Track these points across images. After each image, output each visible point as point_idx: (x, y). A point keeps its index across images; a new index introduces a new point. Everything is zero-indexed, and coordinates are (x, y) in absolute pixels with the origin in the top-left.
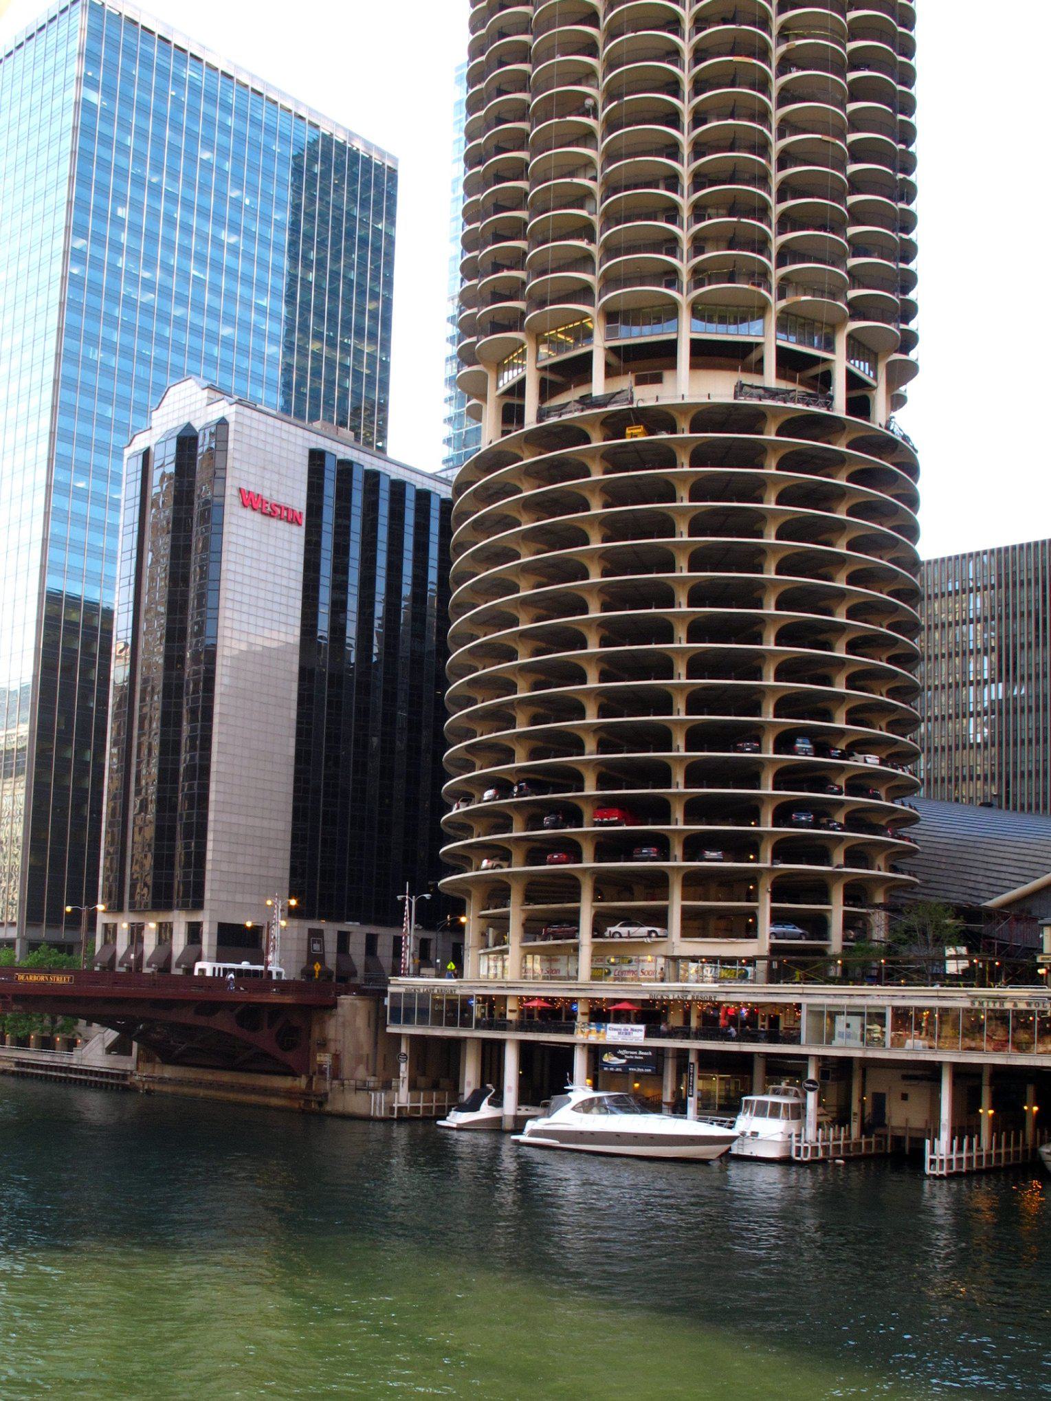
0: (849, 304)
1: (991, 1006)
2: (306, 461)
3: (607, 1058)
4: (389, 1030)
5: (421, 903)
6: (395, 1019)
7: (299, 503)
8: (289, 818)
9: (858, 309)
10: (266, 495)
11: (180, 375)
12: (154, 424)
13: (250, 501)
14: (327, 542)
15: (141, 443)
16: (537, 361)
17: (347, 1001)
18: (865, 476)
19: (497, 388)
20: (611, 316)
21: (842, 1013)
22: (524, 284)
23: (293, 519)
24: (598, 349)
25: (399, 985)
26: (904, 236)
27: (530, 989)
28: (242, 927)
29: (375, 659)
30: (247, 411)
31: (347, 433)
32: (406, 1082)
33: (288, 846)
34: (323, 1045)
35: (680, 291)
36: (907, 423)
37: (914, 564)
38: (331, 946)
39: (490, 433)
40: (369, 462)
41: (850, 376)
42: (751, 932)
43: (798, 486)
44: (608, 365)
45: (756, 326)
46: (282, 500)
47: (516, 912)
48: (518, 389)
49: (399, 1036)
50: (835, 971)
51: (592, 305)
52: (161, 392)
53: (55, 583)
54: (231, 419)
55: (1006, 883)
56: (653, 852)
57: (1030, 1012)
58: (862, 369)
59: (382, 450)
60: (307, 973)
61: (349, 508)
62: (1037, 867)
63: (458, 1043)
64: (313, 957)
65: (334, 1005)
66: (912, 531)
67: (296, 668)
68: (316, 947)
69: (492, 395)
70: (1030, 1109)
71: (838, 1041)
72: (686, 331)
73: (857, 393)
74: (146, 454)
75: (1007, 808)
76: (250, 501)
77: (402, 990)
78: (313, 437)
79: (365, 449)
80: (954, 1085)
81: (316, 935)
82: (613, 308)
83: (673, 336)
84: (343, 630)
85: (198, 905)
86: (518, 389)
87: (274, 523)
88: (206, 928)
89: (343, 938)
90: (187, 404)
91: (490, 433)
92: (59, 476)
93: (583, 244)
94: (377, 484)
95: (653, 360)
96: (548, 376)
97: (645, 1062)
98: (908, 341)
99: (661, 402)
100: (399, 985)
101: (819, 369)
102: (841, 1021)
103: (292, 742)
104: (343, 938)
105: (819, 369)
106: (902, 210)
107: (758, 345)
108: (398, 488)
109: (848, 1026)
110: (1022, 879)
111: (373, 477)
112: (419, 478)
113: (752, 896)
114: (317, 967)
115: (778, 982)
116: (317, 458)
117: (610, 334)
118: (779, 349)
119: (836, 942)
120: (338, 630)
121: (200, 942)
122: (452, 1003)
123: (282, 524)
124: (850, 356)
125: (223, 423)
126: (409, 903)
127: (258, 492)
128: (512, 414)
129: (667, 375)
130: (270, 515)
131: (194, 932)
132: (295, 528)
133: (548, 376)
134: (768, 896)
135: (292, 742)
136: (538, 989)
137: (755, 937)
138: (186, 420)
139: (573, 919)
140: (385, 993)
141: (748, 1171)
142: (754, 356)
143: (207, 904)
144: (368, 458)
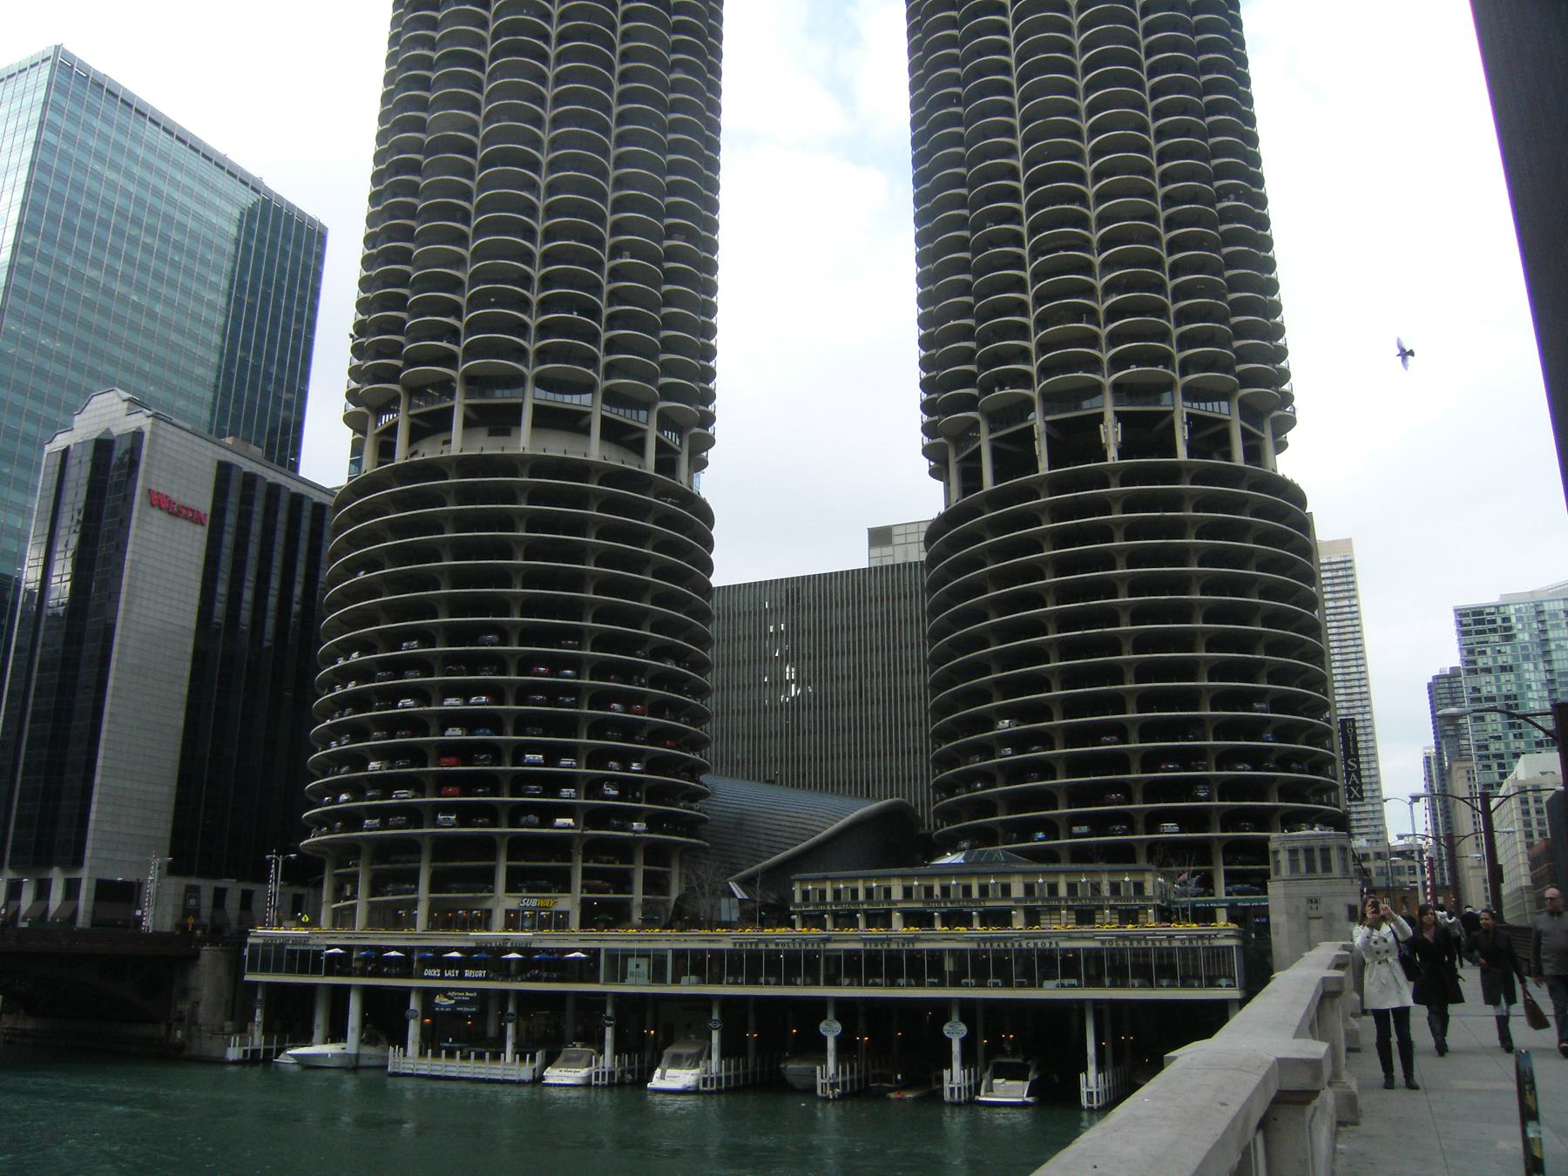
2: (214, 472)
3: (438, 999)
5: (287, 862)
6: (253, 969)
7: (205, 505)
8: (174, 783)
9: (668, 392)
10: (174, 496)
11: (109, 384)
12: (75, 426)
13: (157, 501)
15: (61, 441)
17: (207, 953)
20: (471, 380)
22: (402, 346)
23: (197, 519)
25: (260, 934)
28: (115, 882)
29: (266, 644)
30: (162, 424)
33: (171, 809)
34: (185, 992)
37: (708, 590)
38: (207, 901)
39: (369, 465)
40: (272, 475)
42: (566, 888)
46: (188, 502)
48: (392, 430)
50: (527, 924)
51: (456, 369)
52: (87, 395)
54: (147, 430)
57: (779, 952)
58: (670, 437)
59: (295, 467)
60: (181, 926)
61: (258, 519)
64: (187, 911)
65: (197, 956)
66: (708, 567)
67: (190, 650)
68: (192, 902)
71: (630, 979)
72: (531, 397)
74: (65, 453)
76: (157, 501)
77: (260, 941)
78: (223, 451)
81: (192, 891)
85: (78, 862)
86: (392, 430)
88: (84, 885)
89: (220, 895)
90: (107, 413)
91: (369, 465)
93: (451, 320)
95: (502, 420)
96: (417, 421)
98: (709, 419)
100: (260, 934)
101: (637, 435)
102: (632, 963)
103: (182, 714)
104: (220, 895)
105: (637, 435)
107: (589, 413)
108: (297, 500)
111: (274, 490)
112: (317, 493)
113: (568, 858)
114: (191, 921)
116: (224, 469)
118: (603, 418)
120: (235, 598)
121: (77, 897)
122: (305, 954)
123: (186, 524)
124: (661, 429)
125: (138, 435)
126: (275, 860)
127: (166, 493)
129: (514, 430)
130: (177, 514)
131: (72, 889)
132: (199, 529)
133: (417, 421)
134: (580, 858)
138: (106, 425)
140: (245, 944)
141: (400, 1082)
142: (584, 422)
143: (87, 863)
144: (271, 473)
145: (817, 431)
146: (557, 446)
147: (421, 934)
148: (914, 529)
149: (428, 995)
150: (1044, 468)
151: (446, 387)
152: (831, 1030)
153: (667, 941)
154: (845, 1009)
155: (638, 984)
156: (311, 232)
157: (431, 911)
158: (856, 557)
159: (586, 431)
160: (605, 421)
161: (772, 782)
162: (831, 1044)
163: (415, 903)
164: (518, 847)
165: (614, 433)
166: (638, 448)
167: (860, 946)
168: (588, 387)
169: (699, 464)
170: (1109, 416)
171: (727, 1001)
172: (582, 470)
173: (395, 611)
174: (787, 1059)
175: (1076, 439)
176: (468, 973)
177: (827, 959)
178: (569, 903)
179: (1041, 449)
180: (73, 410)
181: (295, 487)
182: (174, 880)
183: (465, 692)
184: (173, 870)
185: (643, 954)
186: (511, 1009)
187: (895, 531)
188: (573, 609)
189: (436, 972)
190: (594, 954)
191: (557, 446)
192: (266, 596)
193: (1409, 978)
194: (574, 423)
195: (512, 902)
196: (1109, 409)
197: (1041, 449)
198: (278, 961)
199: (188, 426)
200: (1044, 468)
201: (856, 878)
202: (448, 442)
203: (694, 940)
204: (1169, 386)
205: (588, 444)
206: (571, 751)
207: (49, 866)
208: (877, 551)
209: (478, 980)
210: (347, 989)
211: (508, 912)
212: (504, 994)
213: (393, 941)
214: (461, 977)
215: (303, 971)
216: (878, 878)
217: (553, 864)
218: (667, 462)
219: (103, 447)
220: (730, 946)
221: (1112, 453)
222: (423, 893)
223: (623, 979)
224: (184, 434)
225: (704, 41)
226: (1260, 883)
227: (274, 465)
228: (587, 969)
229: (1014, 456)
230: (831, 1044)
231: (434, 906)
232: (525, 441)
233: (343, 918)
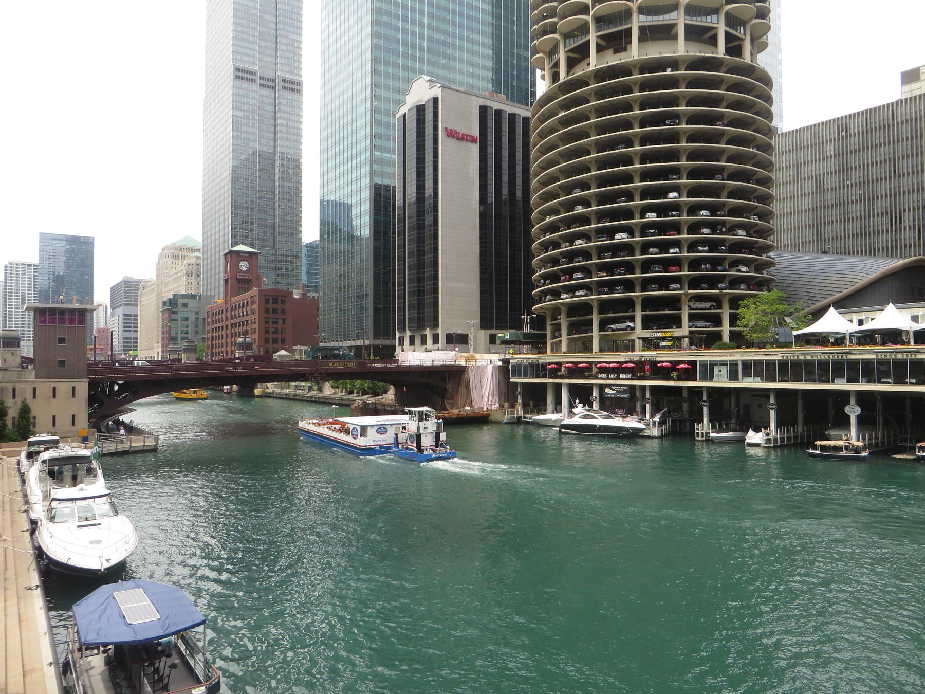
4: (512, 380)
6: (514, 376)
7: (476, 133)
13: (451, 134)
14: (491, 150)
15: (403, 110)
16: (565, 47)
18: (736, 87)
23: (474, 140)
24: (593, 37)
30: (447, 90)
31: (503, 96)
36: (763, 60)
37: (770, 132)
42: (679, 326)
43: (697, 96)
44: (598, 45)
45: (674, 15)
47: (564, 323)
49: (516, 383)
52: (409, 82)
53: (378, 180)
71: (716, 379)
72: (637, 22)
74: (405, 115)
76: (451, 134)
82: (598, 15)
84: (515, 195)
85: (436, 326)
87: (463, 143)
92: (379, 130)
94: (515, 120)
97: (624, 392)
99: (622, 61)
116: (483, 110)
117: (598, 30)
119: (726, 329)
125: (435, 100)
129: (628, 46)
135: (478, 246)
139: (590, 322)
142: (674, 31)
146: (657, 51)
147: (597, 357)
149: (602, 388)
151: (584, 29)
152: (853, 411)
153: (740, 355)
154: (864, 398)
155: (721, 381)
157: (600, 340)
159: (675, 37)
160: (687, 26)
161: (826, 253)
162: (853, 421)
164: (648, 303)
165: (695, 34)
166: (713, 41)
167: (874, 357)
169: (759, 45)
171: (779, 393)
172: (674, 63)
173: (568, 172)
174: (829, 428)
176: (622, 376)
177: (701, 365)
180: (405, 92)
182: (483, 331)
184: (482, 327)
185: (723, 364)
186: (647, 396)
188: (674, 155)
189: (604, 376)
190: (693, 363)
191: (657, 51)
192: (515, 179)
193: (671, 328)
194: (666, 33)
195: (647, 334)
198: (519, 371)
199: (463, 90)
202: (589, 64)
203: (753, 355)
205: (677, 47)
206: (677, 244)
207: (424, 328)
208: (908, 87)
209: (625, 381)
210: (560, 385)
212: (643, 387)
213: (582, 358)
214: (618, 378)
215: (538, 376)
217: (667, 312)
218: (734, 49)
219: (421, 109)
220: (780, 358)
223: (711, 379)
224: (459, 94)
227: (523, 106)
228: (689, 371)
230: (853, 421)
231: (602, 339)
232: (635, 52)
233: (556, 348)
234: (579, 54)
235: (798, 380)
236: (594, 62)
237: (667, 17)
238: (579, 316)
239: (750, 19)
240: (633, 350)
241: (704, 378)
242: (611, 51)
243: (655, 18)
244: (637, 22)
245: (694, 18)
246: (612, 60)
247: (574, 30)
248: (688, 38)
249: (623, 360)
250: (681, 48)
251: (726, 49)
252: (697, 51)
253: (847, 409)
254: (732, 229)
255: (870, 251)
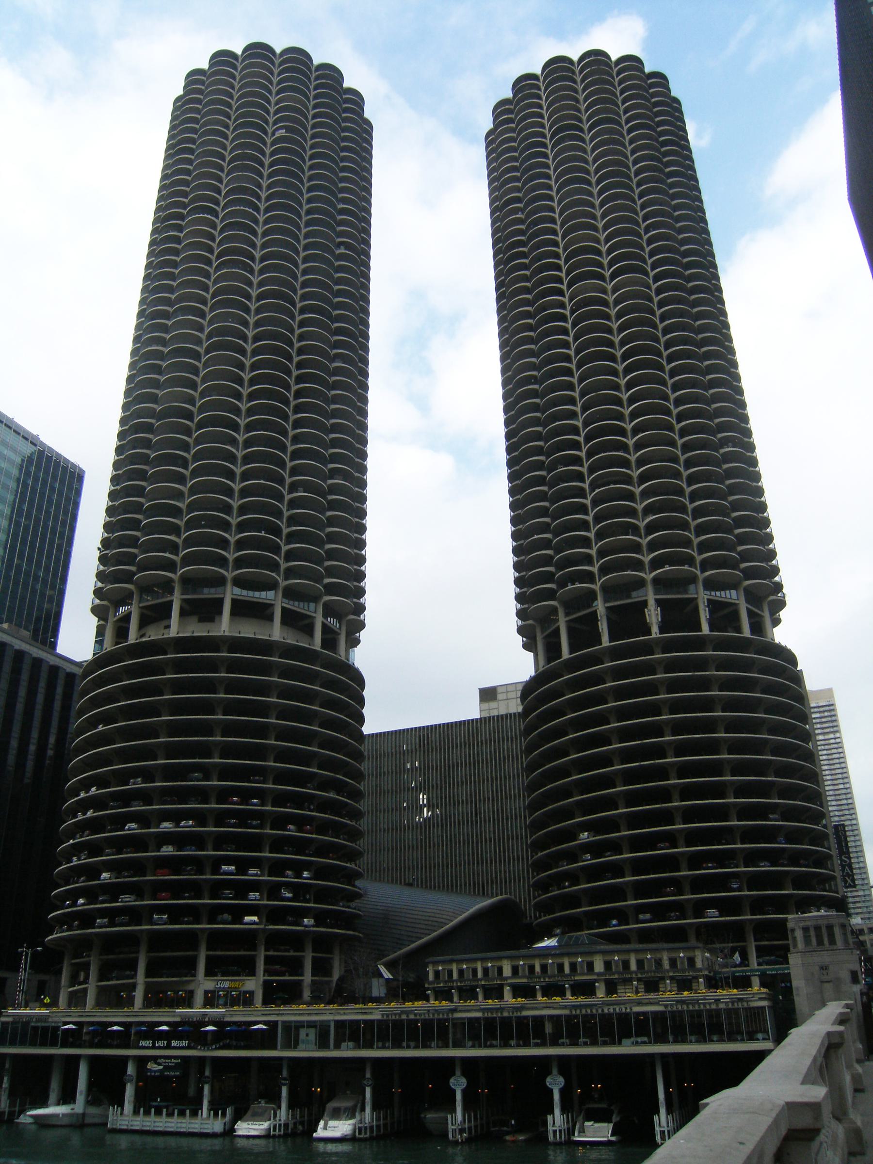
0: (730, 503)
1: (394, 1017)
3: (151, 1066)
5: (35, 955)
9: (331, 589)
19: (115, 616)
21: (303, 1027)
26: (355, 600)
27: (101, 1016)
32: (7, 1092)
35: (227, 570)
40: (36, 652)
41: (324, 626)
42: (252, 973)
45: (271, 594)
48: (127, 618)
50: (221, 1002)
51: (175, 573)
55: (418, 935)
56: (227, 916)
59: (54, 645)
62: (436, 924)
63: (78, 1058)
69: (111, 619)
70: (483, 1091)
71: (301, 1046)
72: (230, 593)
73: (329, 636)
75: (422, 887)
77: (10, 1019)
79: (41, 646)
80: (91, 1074)
83: (222, 596)
86: (127, 618)
93: (172, 538)
95: (208, 611)
96: (145, 611)
97: (176, 1067)
101: (306, 622)
102: (303, 1033)
105: (306, 622)
106: (356, 538)
109: (307, 1035)
110: (427, 932)
112: (69, 665)
115: (150, 1008)
124: (325, 616)
128: (122, 632)
136: (106, 1016)
137: (254, 975)
145: (439, 613)
146: (248, 630)
147: (138, 1012)
148: (512, 688)
149: (141, 1062)
150: (606, 642)
151: (167, 586)
152: (458, 1084)
155: (306, 1051)
156: (72, 474)
158: (470, 710)
159: (270, 618)
161: (410, 885)
162: (459, 1096)
163: (133, 987)
165: (290, 619)
166: (308, 630)
167: (479, 1015)
168: (272, 586)
170: (651, 602)
172: (267, 647)
175: (628, 619)
176: (174, 1043)
178: (253, 984)
179: (603, 627)
181: (52, 660)
183: (176, 817)
185: (311, 1025)
187: (499, 690)
189: (149, 1043)
190: (273, 1025)
191: (248, 630)
194: (261, 612)
196: (651, 597)
197: (603, 627)
200: (606, 642)
201: (475, 960)
204: (693, 579)
209: (180, 1050)
211: (206, 992)
213: (115, 1018)
214: (169, 1047)
216: (492, 959)
218: (330, 641)
220: (379, 1017)
221: (655, 629)
222: (141, 978)
225: (357, 341)
226: (782, 954)
229: (584, 632)
230: (459, 1096)
232: (225, 626)
234: (157, 614)
235: (397, 1045)
236: (175, 628)
237: (263, 594)
238: (117, 956)
239: (347, 615)
240: (190, 1006)
241: (287, 1046)
242: (195, 618)
243: (251, 593)
244: (230, 593)
245: (291, 602)
246: (197, 630)
247: (154, 585)
248: (284, 622)
249: (178, 1019)
250: (276, 632)
251: (323, 640)
252: (292, 639)
253: (549, 1080)
254: (699, 908)
255: (450, 886)
